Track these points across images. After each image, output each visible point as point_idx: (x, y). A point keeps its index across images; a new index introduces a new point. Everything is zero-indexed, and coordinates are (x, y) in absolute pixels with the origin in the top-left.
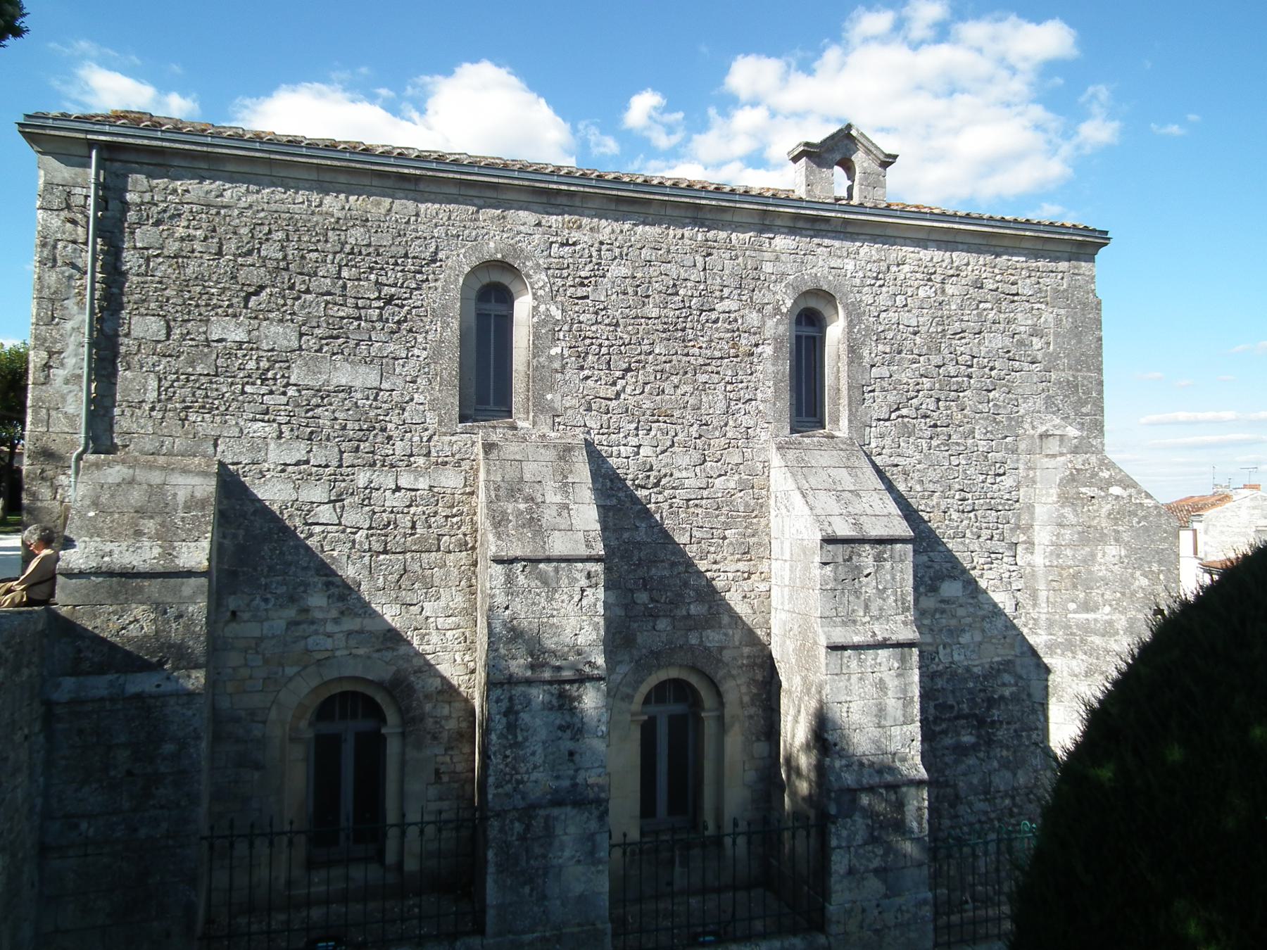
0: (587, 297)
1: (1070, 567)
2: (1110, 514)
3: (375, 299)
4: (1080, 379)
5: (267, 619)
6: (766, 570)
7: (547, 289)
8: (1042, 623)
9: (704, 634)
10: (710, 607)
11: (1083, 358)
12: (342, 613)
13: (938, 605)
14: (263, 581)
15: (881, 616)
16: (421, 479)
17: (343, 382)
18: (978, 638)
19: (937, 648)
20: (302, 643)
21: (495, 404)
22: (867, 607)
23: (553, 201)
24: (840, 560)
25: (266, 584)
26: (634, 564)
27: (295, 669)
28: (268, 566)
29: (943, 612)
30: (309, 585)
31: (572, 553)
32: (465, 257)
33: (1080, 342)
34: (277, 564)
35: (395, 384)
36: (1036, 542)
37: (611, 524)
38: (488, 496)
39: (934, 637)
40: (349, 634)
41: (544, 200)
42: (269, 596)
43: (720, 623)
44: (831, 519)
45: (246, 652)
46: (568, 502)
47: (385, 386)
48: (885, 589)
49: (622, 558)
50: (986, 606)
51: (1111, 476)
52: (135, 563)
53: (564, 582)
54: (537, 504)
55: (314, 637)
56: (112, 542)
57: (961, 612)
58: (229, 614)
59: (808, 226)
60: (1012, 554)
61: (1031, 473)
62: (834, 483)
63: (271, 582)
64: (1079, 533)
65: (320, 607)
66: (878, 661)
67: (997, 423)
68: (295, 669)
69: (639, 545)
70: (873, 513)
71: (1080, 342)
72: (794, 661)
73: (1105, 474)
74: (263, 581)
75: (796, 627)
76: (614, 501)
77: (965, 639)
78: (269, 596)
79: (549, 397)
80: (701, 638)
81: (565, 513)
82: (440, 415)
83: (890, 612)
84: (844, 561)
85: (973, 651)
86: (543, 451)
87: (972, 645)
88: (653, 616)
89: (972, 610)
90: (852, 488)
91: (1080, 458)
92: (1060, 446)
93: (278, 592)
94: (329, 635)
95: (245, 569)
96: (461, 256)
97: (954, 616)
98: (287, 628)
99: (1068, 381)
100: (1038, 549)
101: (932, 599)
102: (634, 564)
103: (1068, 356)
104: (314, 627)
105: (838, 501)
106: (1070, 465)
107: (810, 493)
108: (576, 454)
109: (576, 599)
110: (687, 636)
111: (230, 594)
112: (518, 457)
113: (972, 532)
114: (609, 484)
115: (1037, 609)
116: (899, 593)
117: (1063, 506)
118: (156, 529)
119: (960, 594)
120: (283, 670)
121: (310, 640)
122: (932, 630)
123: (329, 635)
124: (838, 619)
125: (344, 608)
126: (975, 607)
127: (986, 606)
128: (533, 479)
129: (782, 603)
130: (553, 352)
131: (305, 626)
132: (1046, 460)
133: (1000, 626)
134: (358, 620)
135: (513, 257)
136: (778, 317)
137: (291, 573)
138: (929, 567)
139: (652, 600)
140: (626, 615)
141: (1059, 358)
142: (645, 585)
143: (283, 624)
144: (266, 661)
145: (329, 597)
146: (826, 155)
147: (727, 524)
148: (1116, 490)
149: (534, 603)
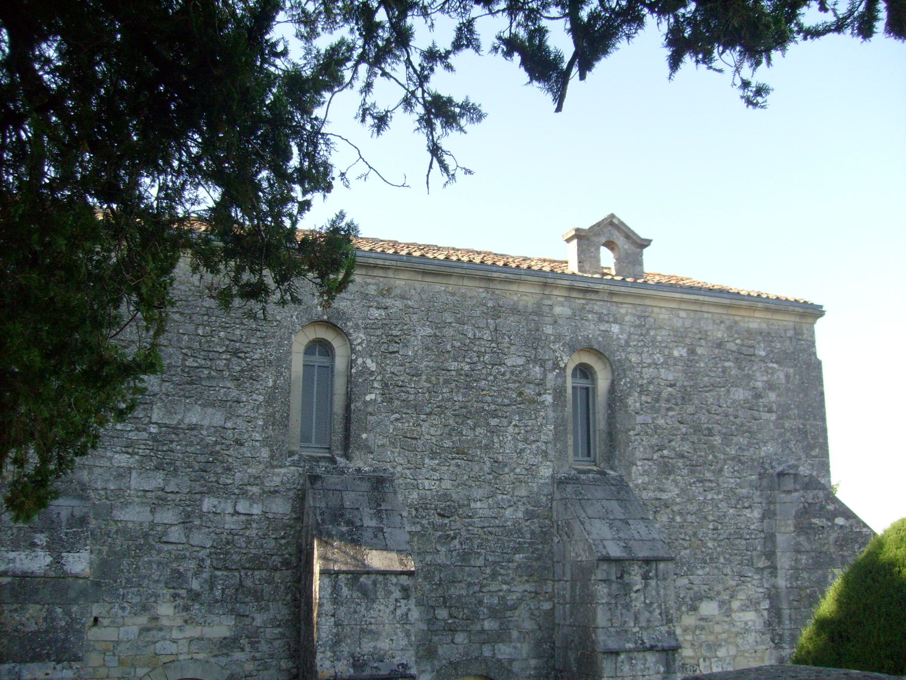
0: (397, 352)
1: (807, 588)
2: (836, 541)
3: (223, 352)
4: (808, 427)
5: (124, 625)
6: (550, 590)
7: (364, 345)
8: (787, 638)
9: (496, 647)
10: (502, 624)
11: (810, 409)
12: (186, 621)
13: (698, 623)
14: (121, 591)
15: (648, 627)
16: (255, 506)
17: (194, 421)
18: (733, 651)
19: (698, 660)
20: (152, 647)
21: (316, 443)
22: (636, 619)
23: (370, 273)
24: (613, 577)
25: (124, 595)
26: (436, 584)
27: (146, 670)
28: (126, 579)
29: (702, 628)
30: (159, 596)
31: (388, 569)
32: (297, 318)
33: (806, 395)
34: (134, 577)
35: (236, 423)
36: (779, 566)
37: (416, 548)
38: (592, 465)
39: (694, 650)
40: (191, 640)
41: (364, 273)
42: (126, 605)
43: (510, 637)
44: (605, 543)
45: (333, 615)
46: (382, 526)
47: (229, 425)
48: (651, 603)
49: (425, 578)
50: (739, 624)
51: (835, 508)
52: (34, 569)
53: (381, 594)
54: (356, 527)
55: (162, 642)
56: (13, 551)
57: (718, 628)
58: (92, 619)
59: (581, 296)
60: (759, 577)
61: (772, 507)
62: (607, 513)
63: (128, 593)
64: (812, 558)
65: (168, 616)
66: (647, 666)
67: (743, 463)
68: (146, 670)
69: (441, 567)
70: (639, 538)
71: (806, 395)
72: (575, 669)
73: (831, 507)
74: (121, 591)
75: (576, 638)
76: (419, 528)
77: (721, 653)
78: (126, 605)
79: (364, 436)
80: (494, 650)
81: (380, 535)
82: (272, 451)
83: (656, 624)
84: (617, 578)
85: (729, 664)
86: (358, 482)
87: (728, 659)
88: (453, 630)
89: (726, 627)
90: (622, 517)
91: (810, 495)
92: (794, 483)
93: (134, 601)
94: (175, 641)
95: (107, 580)
96: (294, 317)
97: (712, 633)
98: (140, 634)
99: (799, 428)
100: (780, 573)
101: (693, 617)
102: (436, 584)
103: (798, 407)
104: (162, 633)
105: (611, 528)
106: (803, 500)
107: (587, 520)
108: (387, 485)
109: (392, 608)
110: (481, 649)
111: (94, 602)
112: (338, 487)
113: (724, 558)
114: (414, 513)
115: (782, 626)
116: (663, 607)
117: (798, 535)
118: (47, 541)
119: (716, 612)
120: (135, 671)
121: (158, 645)
122: (693, 645)
123: (175, 641)
124: (612, 630)
125: (188, 617)
126: (729, 624)
127: (739, 624)
128: (352, 506)
129: (565, 619)
130: (368, 398)
131: (154, 632)
132: (783, 495)
133: (751, 641)
134: (199, 628)
135: (336, 318)
136: (557, 371)
137: (144, 585)
138: (690, 589)
139: (451, 616)
140: (429, 630)
141: (789, 409)
142: (445, 603)
143: (136, 629)
144: (121, 663)
145: (175, 607)
146: (594, 239)
147: (516, 549)
148: (840, 521)
149: (355, 612)
